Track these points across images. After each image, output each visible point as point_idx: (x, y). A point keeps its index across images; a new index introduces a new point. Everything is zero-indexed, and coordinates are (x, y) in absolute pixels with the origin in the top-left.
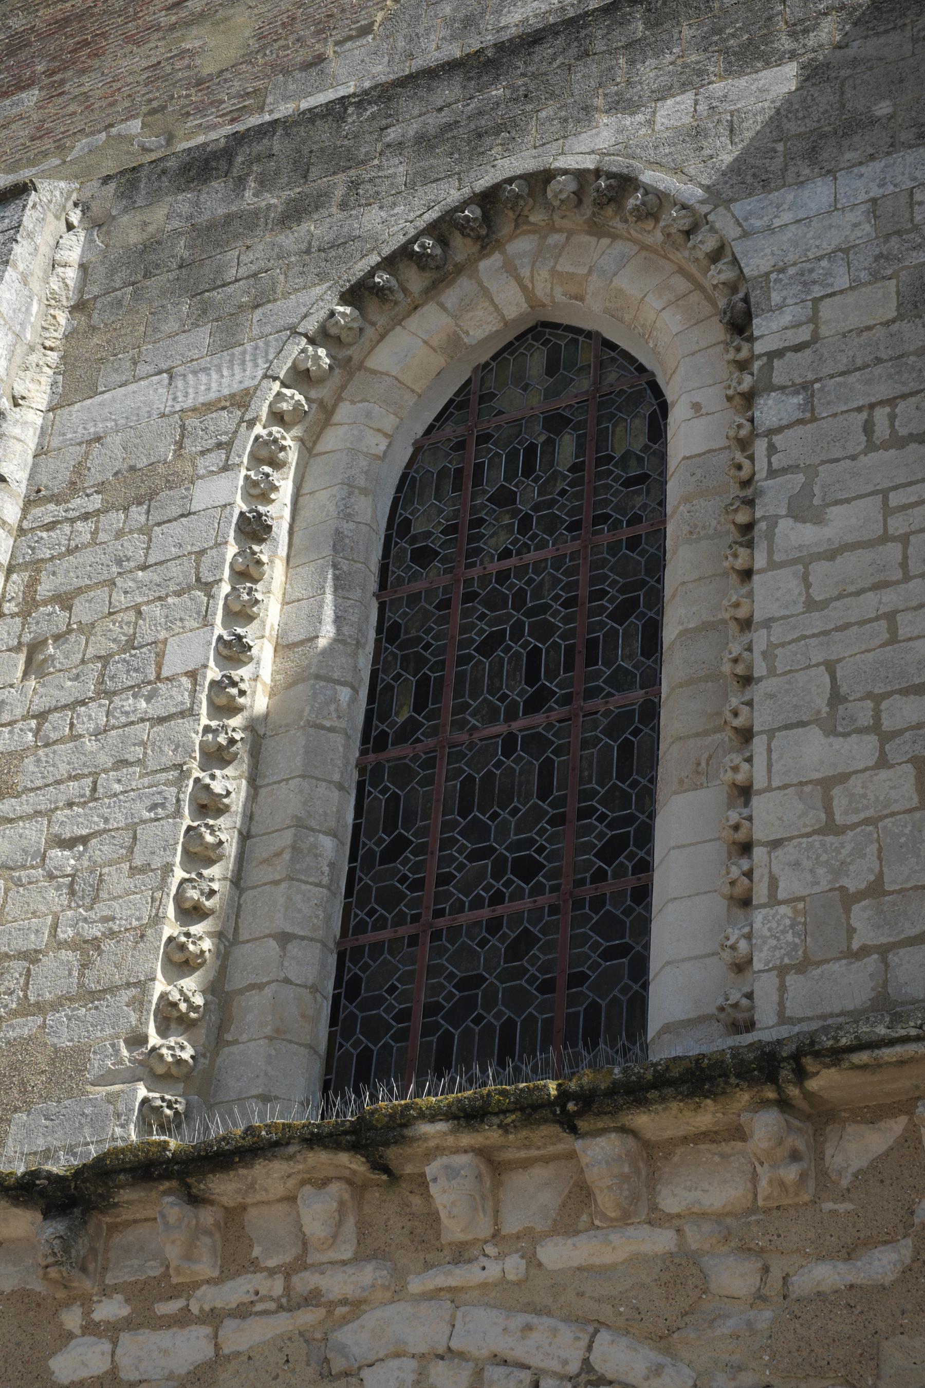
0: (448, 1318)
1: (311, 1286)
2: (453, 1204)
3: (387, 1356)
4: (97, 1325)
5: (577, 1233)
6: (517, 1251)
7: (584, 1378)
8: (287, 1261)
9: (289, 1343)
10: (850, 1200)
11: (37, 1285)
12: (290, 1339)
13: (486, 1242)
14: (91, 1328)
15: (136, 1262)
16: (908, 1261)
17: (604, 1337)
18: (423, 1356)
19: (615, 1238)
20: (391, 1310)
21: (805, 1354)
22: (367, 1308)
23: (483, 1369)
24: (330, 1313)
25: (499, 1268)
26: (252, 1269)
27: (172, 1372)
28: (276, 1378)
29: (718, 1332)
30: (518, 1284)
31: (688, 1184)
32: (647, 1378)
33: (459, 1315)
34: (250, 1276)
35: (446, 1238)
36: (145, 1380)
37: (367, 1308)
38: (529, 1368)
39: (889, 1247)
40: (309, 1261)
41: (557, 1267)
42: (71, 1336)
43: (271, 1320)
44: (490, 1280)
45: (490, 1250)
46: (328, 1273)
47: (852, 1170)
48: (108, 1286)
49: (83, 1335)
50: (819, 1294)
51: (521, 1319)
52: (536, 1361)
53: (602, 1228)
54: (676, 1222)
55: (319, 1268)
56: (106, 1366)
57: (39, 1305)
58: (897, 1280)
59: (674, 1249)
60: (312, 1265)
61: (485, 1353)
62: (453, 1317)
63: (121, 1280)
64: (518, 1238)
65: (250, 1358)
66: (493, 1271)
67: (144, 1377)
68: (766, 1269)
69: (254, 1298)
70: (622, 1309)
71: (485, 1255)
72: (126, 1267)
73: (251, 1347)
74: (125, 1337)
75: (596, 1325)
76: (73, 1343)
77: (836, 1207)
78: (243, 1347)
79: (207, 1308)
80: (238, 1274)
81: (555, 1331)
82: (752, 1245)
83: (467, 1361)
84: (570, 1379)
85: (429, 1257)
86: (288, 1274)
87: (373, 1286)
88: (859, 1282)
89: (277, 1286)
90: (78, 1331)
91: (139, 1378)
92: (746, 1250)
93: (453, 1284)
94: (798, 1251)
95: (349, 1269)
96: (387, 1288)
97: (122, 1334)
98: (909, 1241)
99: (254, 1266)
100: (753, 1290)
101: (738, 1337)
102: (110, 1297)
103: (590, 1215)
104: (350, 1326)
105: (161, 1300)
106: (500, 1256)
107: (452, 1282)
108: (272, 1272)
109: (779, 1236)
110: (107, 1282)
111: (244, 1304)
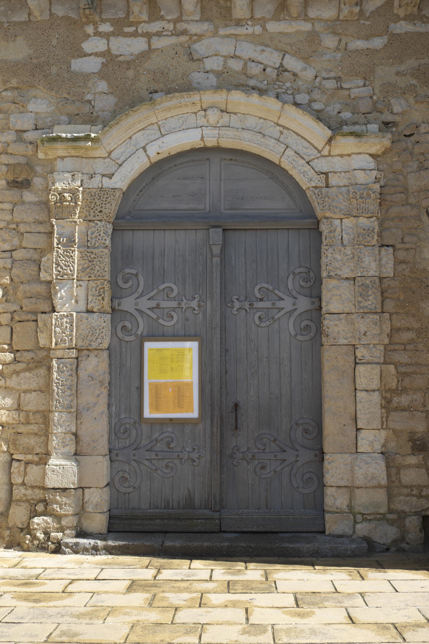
0: (234, 44)
1: (184, 28)
2: (243, 5)
3: (212, 55)
4: (101, 33)
5: (280, 20)
6: (259, 24)
7: (281, 69)
8: (175, 18)
9: (176, 47)
10: (369, 21)
11: (73, 15)
12: (176, 46)
13: (248, 20)
14: (97, 34)
15: (113, 11)
16: (386, 43)
17: (287, 56)
18: (225, 56)
19: (293, 24)
20: (213, 40)
21: (352, 68)
22: (204, 38)
23: (332, 71)
24: (191, 38)
25: (252, 29)
26: (161, 19)
27: (132, 53)
28: (173, 58)
29: (324, 59)
30: (259, 35)
31: (318, 8)
32: (301, 71)
33: (238, 44)
34: (160, 22)
35: (234, 16)
36: (123, 55)
37: (204, 38)
38: (262, 64)
39: (380, 37)
40: (183, 19)
41: (273, 31)
42: (89, 36)
43: (170, 38)
44: (249, 33)
45: (249, 23)
46: (191, 24)
47: (370, 11)
48: (103, 19)
49: (94, 36)
50: (357, 50)
51: (260, 48)
52: (265, 62)
53: (288, 20)
54: (312, 21)
55: (187, 21)
56: (106, 48)
57: (75, 23)
58: (382, 48)
59: (311, 30)
60: (184, 20)
61: (247, 58)
62: (236, 45)
63: (108, 17)
64: (259, 20)
65: (162, 51)
66: (250, 30)
67: (122, 54)
68: (340, 40)
69: (163, 30)
70: (294, 48)
71: (247, 24)
72: (110, 12)
73: (162, 47)
74: (112, 39)
75: (284, 52)
76: (90, 39)
77: (365, 22)
78: (160, 47)
79: (145, 31)
80: (155, 21)
81: (272, 53)
82: (337, 32)
83: (241, 59)
84: (276, 69)
85: (227, 23)
86: (175, 23)
87: (207, 30)
88: (370, 47)
89: (171, 26)
90: (92, 34)
91: (120, 54)
92: (335, 33)
93: (237, 33)
94: (352, 36)
95: (199, 24)
96: (212, 31)
97: (111, 37)
98: (387, 37)
99: (162, 18)
100: (335, 46)
101: (330, 61)
102: (105, 23)
103: (284, 15)
104: (198, 43)
105: (126, 26)
106: (253, 25)
107: (236, 32)
108: (169, 21)
109: (346, 30)
110: (103, 17)
111: (159, 32)
